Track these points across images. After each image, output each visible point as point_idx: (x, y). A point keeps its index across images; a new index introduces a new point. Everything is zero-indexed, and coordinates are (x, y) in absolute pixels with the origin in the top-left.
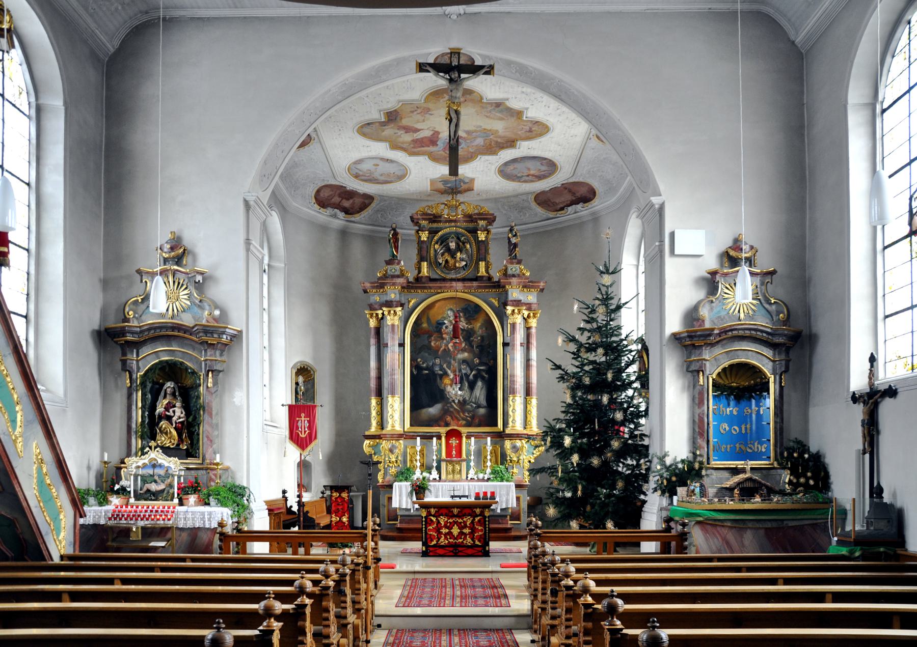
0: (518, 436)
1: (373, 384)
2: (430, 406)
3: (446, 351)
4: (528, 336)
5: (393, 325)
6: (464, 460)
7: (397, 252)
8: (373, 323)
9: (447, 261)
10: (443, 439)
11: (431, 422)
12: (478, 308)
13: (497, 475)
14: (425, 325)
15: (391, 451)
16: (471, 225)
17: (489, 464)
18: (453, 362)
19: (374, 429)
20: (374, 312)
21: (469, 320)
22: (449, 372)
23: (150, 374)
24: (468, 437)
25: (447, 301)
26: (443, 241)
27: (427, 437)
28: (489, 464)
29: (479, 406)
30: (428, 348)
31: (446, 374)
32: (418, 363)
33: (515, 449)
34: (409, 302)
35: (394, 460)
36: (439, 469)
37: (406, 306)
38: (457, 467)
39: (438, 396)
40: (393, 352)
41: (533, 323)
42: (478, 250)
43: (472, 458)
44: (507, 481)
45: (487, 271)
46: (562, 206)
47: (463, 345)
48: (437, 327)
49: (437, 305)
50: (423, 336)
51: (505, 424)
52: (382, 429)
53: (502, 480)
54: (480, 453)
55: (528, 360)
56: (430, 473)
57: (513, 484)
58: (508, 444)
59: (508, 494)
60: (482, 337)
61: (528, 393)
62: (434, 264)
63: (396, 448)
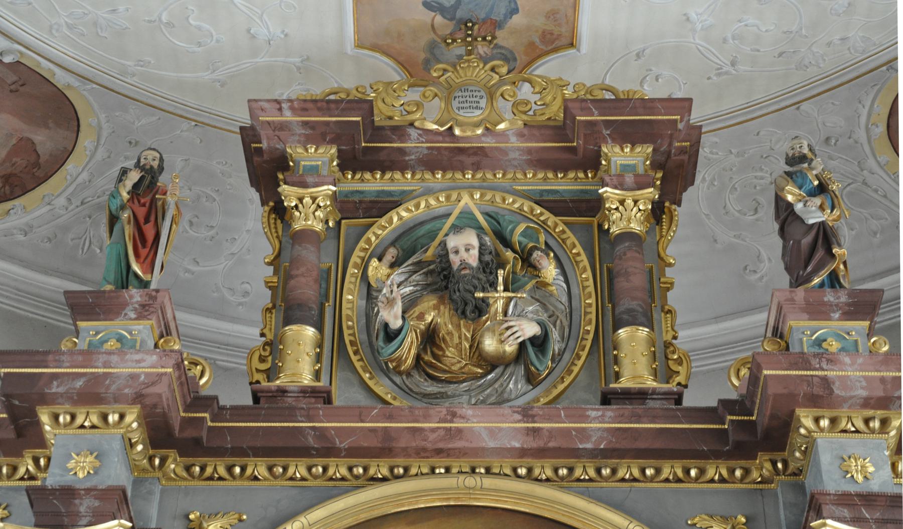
16: (565, 184)
42: (609, 284)
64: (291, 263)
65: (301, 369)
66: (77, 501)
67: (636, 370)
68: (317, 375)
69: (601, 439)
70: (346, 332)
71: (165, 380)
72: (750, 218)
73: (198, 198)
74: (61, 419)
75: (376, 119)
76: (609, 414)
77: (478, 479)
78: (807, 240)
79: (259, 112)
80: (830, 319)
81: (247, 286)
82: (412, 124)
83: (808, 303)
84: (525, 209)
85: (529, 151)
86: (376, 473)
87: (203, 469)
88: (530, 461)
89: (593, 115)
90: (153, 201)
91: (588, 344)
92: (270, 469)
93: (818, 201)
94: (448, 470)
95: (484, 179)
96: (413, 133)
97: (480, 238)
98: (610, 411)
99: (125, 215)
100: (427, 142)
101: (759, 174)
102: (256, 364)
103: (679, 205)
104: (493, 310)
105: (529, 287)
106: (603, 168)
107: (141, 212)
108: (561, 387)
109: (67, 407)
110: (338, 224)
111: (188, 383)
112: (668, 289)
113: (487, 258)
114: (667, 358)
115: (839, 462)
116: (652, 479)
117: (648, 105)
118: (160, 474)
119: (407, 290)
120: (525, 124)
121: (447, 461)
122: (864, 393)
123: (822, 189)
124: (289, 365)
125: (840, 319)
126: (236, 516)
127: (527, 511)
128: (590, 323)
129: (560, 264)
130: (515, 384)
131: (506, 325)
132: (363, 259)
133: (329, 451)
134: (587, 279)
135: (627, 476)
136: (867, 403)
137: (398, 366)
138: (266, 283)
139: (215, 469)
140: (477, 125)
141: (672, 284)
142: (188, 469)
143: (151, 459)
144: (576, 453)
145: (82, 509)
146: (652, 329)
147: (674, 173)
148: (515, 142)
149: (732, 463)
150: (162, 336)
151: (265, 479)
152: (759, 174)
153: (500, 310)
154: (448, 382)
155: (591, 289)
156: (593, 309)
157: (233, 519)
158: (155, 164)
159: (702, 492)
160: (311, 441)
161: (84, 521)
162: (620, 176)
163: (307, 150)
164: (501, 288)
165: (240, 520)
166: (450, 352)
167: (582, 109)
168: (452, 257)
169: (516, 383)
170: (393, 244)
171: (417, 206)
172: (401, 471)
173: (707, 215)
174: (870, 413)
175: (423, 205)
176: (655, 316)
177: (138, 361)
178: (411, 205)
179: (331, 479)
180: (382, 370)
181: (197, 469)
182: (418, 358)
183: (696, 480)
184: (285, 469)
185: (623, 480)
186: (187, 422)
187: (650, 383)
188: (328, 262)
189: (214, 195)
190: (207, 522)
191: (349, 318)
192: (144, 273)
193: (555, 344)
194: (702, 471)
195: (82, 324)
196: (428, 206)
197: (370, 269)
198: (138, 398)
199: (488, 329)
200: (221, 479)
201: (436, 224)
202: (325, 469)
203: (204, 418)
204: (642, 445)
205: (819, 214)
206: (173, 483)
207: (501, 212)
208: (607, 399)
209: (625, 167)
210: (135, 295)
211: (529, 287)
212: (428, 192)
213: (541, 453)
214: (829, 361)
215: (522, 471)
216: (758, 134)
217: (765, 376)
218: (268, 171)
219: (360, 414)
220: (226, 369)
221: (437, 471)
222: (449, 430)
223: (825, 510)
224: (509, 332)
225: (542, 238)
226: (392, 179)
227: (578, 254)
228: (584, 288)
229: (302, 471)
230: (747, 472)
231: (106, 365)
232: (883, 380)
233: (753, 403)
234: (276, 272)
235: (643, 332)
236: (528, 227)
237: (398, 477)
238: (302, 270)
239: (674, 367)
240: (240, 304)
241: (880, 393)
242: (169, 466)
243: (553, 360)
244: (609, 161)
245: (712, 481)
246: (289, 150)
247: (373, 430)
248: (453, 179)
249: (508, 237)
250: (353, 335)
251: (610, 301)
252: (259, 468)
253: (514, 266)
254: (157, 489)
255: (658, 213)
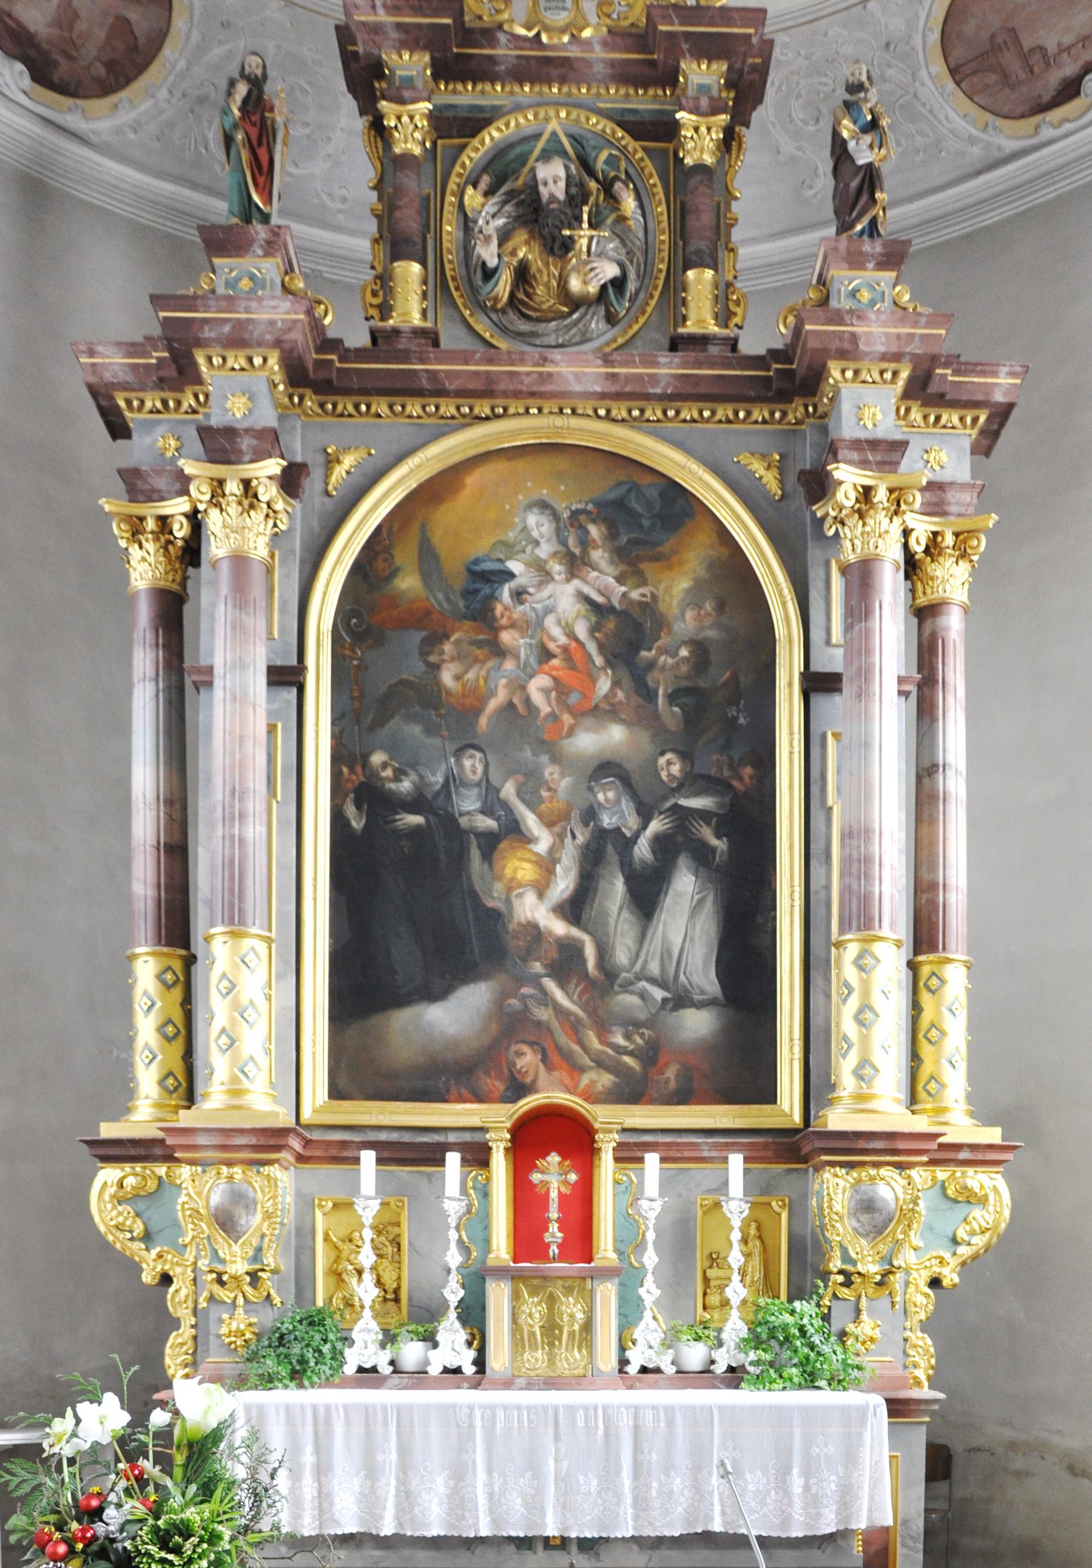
0: (892, 1148)
1: (143, 879)
2: (433, 994)
4: (927, 653)
5: (239, 561)
6: (608, 1273)
7: (268, 200)
8: (145, 568)
9: (523, 275)
10: (500, 1164)
11: (434, 1079)
12: (677, 506)
13: (787, 1355)
14: (408, 583)
15: (226, 1223)
16: (644, 102)
17: (736, 1292)
18: (550, 772)
19: (142, 1119)
20: (151, 511)
21: (632, 559)
22: (531, 822)
24: (629, 1154)
25: (521, 465)
26: (504, 171)
27: (415, 1153)
28: (736, 1292)
29: (681, 1000)
30: (425, 698)
31: (513, 830)
32: (373, 775)
33: (873, 1217)
34: (331, 462)
35: (239, 1267)
36: (473, 1315)
37: (312, 485)
38: (572, 1309)
40: (238, 699)
41: (952, 580)
42: (681, 215)
43: (650, 1258)
44: (836, 1382)
45: (724, 317)
46: (1069, 68)
47: (604, 685)
48: (468, 594)
49: (472, 480)
50: (400, 634)
51: (816, 1088)
52: (190, 1099)
53: (810, 1380)
54: (684, 1239)
55: (925, 774)
56: (430, 1339)
57: (877, 1402)
58: (835, 1187)
59: (850, 1458)
60: (699, 647)
61: (925, 935)
62: (459, 284)
63: (250, 1205)
64: (395, 189)
65: (410, 310)
66: (238, 440)
67: (701, 318)
68: (424, 313)
69: (669, 384)
70: (447, 266)
71: (299, 326)
72: (811, 128)
73: (292, 90)
74: (215, 361)
75: (467, 18)
76: (677, 360)
78: (854, 184)
79: (354, 10)
80: (864, 269)
81: (344, 191)
82: (500, 27)
83: (849, 252)
84: (608, 131)
85: (612, 64)
87: (335, 406)
88: (608, 403)
89: (672, 24)
90: (263, 119)
91: (661, 283)
92: (391, 407)
93: (867, 139)
94: (540, 410)
95: (569, 94)
96: (502, 38)
97: (567, 168)
98: (677, 358)
99: (240, 136)
100: (516, 48)
101: (824, 80)
102: (370, 299)
103: (748, 127)
104: (577, 246)
105: (609, 221)
106: (680, 86)
107: (254, 133)
108: (636, 327)
109: (219, 350)
110: (434, 144)
111: (316, 325)
112: (732, 225)
113: (573, 190)
114: (727, 299)
115: (856, 410)
116: (708, 421)
117: (726, 14)
118: (298, 411)
119: (501, 222)
120: (609, 31)
121: (540, 402)
122: (881, 349)
123: (873, 125)
124: (399, 303)
125: (874, 269)
128: (662, 261)
129: (639, 198)
130: (596, 324)
131: (589, 267)
132: (458, 185)
133: (440, 392)
134: (661, 214)
136: (884, 357)
137: (496, 303)
138: (372, 210)
140: (563, 31)
141: (736, 220)
142: (322, 406)
143: (291, 397)
144: (647, 397)
145: (244, 447)
146: (716, 270)
147: (745, 93)
148: (599, 53)
149: (773, 406)
150: (286, 273)
152: (824, 80)
153: (585, 249)
154: (539, 320)
155: (665, 224)
156: (666, 247)
158: (259, 72)
159: (748, 432)
160: (425, 383)
161: (247, 458)
162: (697, 99)
163: (401, 57)
164: (585, 225)
165: (370, 454)
166: (540, 290)
167: (664, 17)
168: (541, 188)
169: (597, 323)
170: (485, 169)
171: (507, 125)
172: (501, 411)
173: (773, 124)
174: (885, 365)
175: (513, 124)
176: (720, 255)
177: (274, 307)
178: (501, 123)
179: (442, 417)
180: (480, 307)
181: (330, 406)
182: (512, 295)
183: (744, 421)
185: (685, 421)
186: (319, 364)
187: (713, 329)
188: (428, 189)
189: (307, 87)
191: (450, 252)
192: (264, 204)
193: (631, 286)
194: (749, 413)
195: (217, 261)
196: (517, 125)
197: (466, 197)
198: (278, 343)
199: (574, 269)
200: (350, 416)
201: (525, 148)
203: (332, 361)
204: (702, 390)
205: (868, 153)
207: (584, 133)
208: (675, 344)
209: (702, 88)
210: (260, 231)
211: (609, 221)
212: (518, 108)
213: (618, 396)
214: (859, 317)
215: (602, 412)
216: (826, 34)
217: (808, 331)
218: (366, 80)
219: (465, 357)
220: (333, 282)
222: (541, 374)
223: (842, 453)
224: (592, 274)
225: (623, 165)
226: (483, 92)
227: (655, 185)
228: (659, 223)
230: (784, 414)
231: (247, 310)
232: (898, 336)
233: (795, 353)
234: (380, 198)
235: (709, 274)
236: (611, 155)
237: (498, 417)
238: (406, 200)
239: (733, 307)
240: (340, 211)
241: (894, 349)
243: (630, 301)
244: (686, 78)
245: (756, 422)
246: (384, 57)
247: (477, 373)
248: (540, 93)
249: (591, 162)
250: (453, 270)
251: (682, 237)
253: (597, 197)
255: (729, 141)
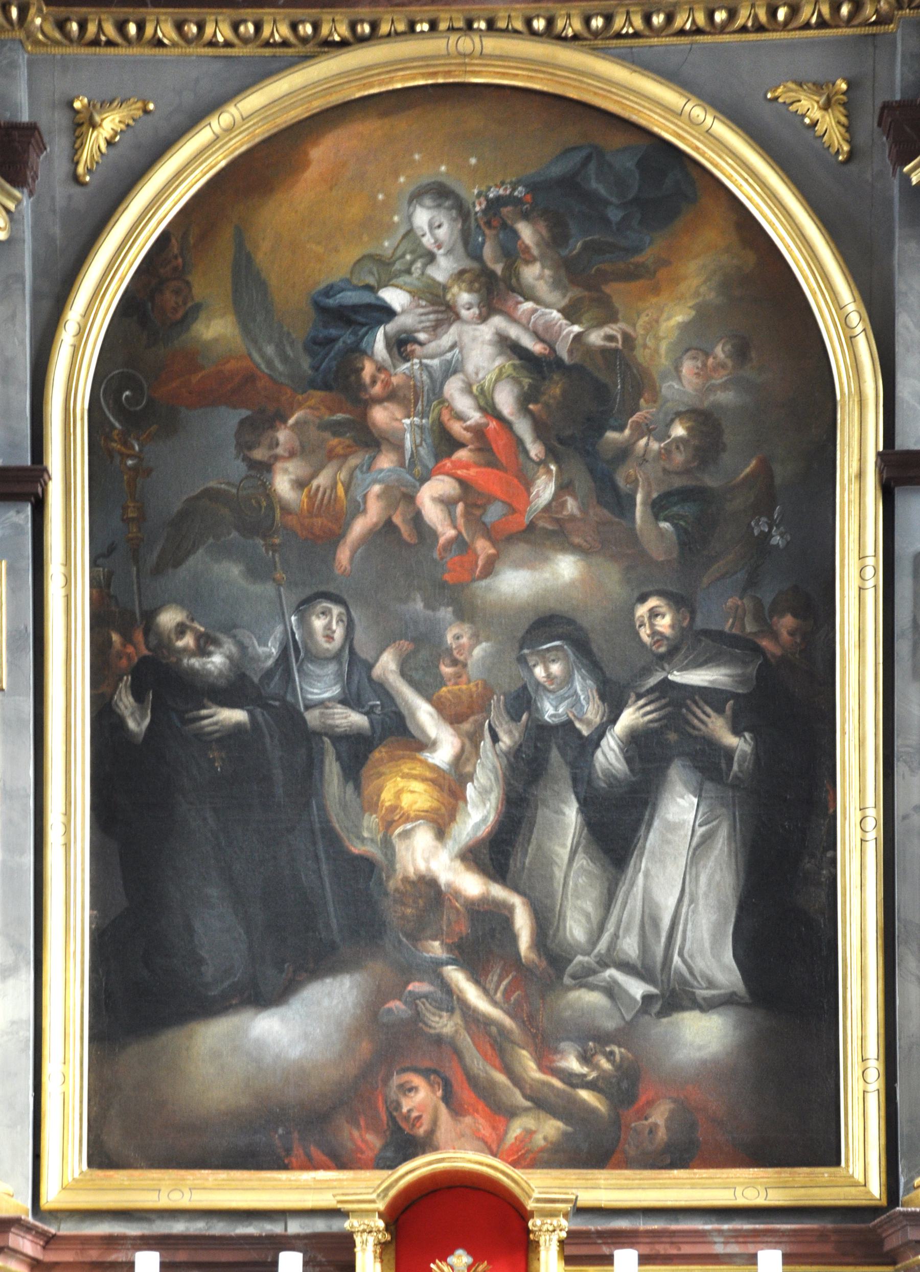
2: (264, 991)
3: (402, 540)
12: (670, 182)
14: (217, 329)
18: (455, 634)
22: (425, 715)
23: (417, 676)
29: (675, 997)
32: (162, 646)
34: (81, 124)
39: (333, 913)
47: (544, 490)
48: (318, 345)
49: (321, 153)
60: (705, 422)
77: (477, 39)
86: (331, 34)
92: (179, 27)
94: (433, 26)
116: (723, 29)
118: (20, 34)
126: (139, 105)
127: (545, 89)
135: (688, 26)
139: (100, 28)
142: (61, 25)
151: (174, 45)
157: (135, 110)
159: (791, 46)
165: (146, 112)
172: (367, 29)
179: (267, 44)
184: (201, 27)
185: (682, 32)
190: (100, 113)
200: (110, 43)
202: (258, 27)
206: (43, 50)
221: (418, 28)
229: (223, 33)
237: (362, 40)
242: (33, 21)
252: (163, 25)
254: (22, 59)
